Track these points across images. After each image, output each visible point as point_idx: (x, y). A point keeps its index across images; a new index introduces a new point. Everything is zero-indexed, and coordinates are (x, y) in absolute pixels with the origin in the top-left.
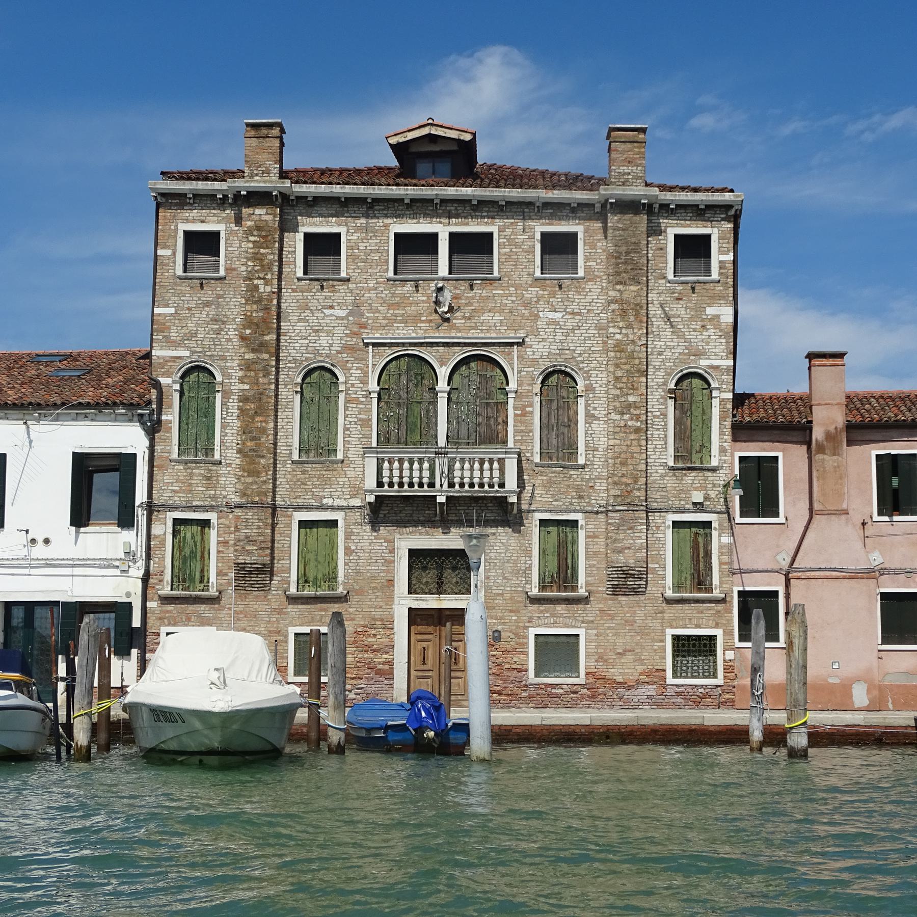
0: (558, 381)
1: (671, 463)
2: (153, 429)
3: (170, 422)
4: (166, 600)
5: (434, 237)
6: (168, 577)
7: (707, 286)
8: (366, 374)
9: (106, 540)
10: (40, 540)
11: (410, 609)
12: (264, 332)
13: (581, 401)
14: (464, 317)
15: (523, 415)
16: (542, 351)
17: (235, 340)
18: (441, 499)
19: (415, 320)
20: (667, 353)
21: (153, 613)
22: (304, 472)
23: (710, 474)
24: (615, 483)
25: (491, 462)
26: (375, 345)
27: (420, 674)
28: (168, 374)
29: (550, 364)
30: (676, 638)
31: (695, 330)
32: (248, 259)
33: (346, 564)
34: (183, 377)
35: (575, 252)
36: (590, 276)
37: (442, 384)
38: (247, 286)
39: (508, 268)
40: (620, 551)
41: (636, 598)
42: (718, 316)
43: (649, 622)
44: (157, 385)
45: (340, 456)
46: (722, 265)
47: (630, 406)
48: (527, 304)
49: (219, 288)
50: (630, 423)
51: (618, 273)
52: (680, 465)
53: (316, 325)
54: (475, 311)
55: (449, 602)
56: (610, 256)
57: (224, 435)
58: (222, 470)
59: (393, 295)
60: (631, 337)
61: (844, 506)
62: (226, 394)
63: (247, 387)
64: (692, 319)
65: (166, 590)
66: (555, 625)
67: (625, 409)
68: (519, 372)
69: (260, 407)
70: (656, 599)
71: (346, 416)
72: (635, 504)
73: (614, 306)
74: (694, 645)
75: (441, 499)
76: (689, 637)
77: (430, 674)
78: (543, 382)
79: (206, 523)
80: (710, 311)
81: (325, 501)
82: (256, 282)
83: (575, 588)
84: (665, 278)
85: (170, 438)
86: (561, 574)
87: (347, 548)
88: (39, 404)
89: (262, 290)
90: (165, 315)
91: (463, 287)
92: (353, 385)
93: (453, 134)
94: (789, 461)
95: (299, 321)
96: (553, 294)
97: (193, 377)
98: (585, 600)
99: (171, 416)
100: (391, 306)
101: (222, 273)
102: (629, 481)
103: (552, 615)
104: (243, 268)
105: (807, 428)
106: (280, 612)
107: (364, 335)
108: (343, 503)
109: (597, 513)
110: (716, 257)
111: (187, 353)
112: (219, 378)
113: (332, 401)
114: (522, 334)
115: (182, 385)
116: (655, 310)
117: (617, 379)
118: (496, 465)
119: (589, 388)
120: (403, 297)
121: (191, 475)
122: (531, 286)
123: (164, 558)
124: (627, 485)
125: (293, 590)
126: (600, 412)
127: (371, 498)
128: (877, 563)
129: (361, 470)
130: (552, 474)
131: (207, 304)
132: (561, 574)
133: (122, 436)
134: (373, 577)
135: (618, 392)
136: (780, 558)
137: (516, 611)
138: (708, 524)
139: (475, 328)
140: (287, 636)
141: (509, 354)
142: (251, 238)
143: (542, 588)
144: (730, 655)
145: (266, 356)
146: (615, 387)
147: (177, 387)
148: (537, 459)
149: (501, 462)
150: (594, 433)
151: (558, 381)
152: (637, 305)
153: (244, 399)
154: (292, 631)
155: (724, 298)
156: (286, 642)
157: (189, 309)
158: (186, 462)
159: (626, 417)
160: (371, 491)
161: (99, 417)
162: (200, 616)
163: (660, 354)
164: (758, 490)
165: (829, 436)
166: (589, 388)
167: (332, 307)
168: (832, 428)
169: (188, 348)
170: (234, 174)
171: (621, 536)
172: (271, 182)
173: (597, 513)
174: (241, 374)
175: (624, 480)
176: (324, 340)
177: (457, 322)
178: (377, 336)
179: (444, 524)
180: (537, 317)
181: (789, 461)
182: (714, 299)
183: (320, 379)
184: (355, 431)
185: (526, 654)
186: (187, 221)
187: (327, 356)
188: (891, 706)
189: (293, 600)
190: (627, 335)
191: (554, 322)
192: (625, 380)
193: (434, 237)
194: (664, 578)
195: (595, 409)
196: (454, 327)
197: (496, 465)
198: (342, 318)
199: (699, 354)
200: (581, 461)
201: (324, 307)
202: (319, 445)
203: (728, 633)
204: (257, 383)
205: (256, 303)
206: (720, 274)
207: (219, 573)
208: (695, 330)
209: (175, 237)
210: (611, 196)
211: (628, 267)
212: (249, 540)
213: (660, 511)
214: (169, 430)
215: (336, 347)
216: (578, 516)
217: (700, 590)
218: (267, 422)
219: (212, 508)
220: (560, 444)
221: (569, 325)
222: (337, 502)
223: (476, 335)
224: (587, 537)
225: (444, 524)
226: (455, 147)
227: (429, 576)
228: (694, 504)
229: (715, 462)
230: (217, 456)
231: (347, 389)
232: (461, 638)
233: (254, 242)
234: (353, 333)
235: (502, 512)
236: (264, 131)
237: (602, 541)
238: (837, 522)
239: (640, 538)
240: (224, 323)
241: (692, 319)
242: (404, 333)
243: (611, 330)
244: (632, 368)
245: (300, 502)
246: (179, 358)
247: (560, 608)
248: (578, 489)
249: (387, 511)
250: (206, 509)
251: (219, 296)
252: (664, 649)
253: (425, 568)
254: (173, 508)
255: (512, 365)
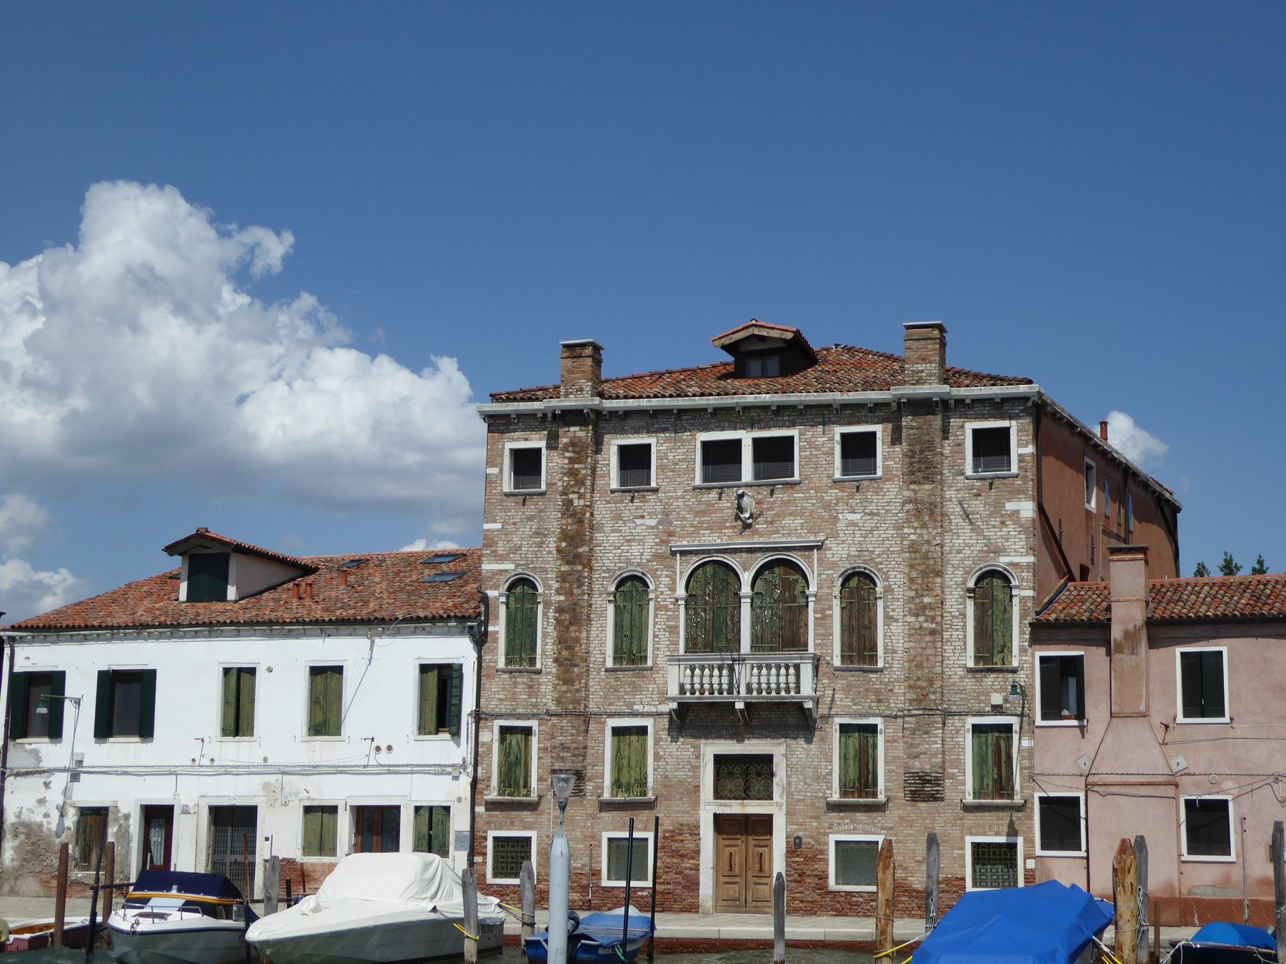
0: (858, 585)
1: (971, 664)
2: (481, 640)
3: (497, 632)
4: (491, 806)
5: (737, 443)
6: (495, 781)
7: (1006, 481)
8: (674, 581)
9: (443, 749)
10: (384, 747)
11: (716, 815)
12: (576, 544)
13: (880, 603)
14: (766, 522)
15: (824, 619)
16: (841, 553)
17: (554, 550)
18: (740, 705)
19: (720, 527)
20: (963, 551)
21: (481, 817)
22: (617, 679)
23: (1010, 675)
24: (910, 687)
25: (787, 667)
26: (683, 553)
27: (727, 880)
28: (496, 587)
29: (849, 566)
30: (976, 846)
31: (994, 527)
32: (564, 474)
33: (655, 770)
34: (509, 589)
35: (873, 454)
36: (888, 477)
37: (746, 590)
38: (563, 501)
39: (808, 471)
40: (916, 757)
41: (936, 804)
42: (1017, 512)
43: (949, 829)
44: (485, 599)
45: (650, 663)
46: (1021, 458)
47: (924, 607)
48: (827, 507)
49: (540, 502)
50: (925, 625)
51: (912, 473)
52: (981, 666)
53: (628, 535)
54: (776, 515)
55: (754, 807)
56: (905, 455)
57: (544, 644)
58: (543, 679)
59: (700, 502)
60: (926, 537)
61: (1143, 708)
62: (547, 605)
63: (562, 598)
64: (991, 515)
65: (493, 795)
66: (855, 831)
67: (919, 611)
68: (819, 575)
69: (573, 617)
70: (956, 805)
71: (655, 623)
72: (929, 707)
73: (908, 506)
74: (994, 853)
75: (740, 705)
76: (989, 845)
77: (737, 879)
78: (843, 585)
79: (527, 731)
80: (1010, 506)
81: (636, 707)
82: (571, 496)
83: (875, 795)
84: (963, 474)
85: (496, 648)
86: (861, 780)
87: (656, 755)
88: (383, 619)
89: (576, 504)
90: (493, 531)
91: (765, 492)
92: (662, 593)
93: (775, 334)
94: (1094, 659)
95: (613, 531)
96: (851, 496)
97: (519, 589)
98: (880, 808)
99: (499, 628)
100: (697, 513)
101: (543, 487)
102: (925, 685)
103: (853, 822)
104: (560, 484)
105: (1106, 626)
106: (594, 817)
107: (672, 544)
108: (653, 709)
109: (896, 717)
110: (1015, 451)
111: (512, 566)
112: (540, 590)
113: (643, 608)
114: (821, 537)
115: (508, 597)
116: (953, 508)
117: (912, 580)
118: (792, 671)
119: (888, 590)
120: (709, 504)
121: (515, 684)
122: (830, 488)
123: (491, 764)
124: (922, 688)
125: (607, 795)
126: (898, 613)
127: (674, 705)
128: (1180, 768)
129: (672, 676)
130: (852, 678)
131: (530, 518)
132: (861, 780)
133: (455, 649)
134: (681, 782)
135: (913, 594)
136: (1081, 762)
137: (816, 818)
138: (1008, 728)
139: (777, 532)
140: (600, 841)
141: (810, 557)
142: (567, 455)
143: (844, 793)
144: (1031, 864)
145: (579, 568)
146: (910, 589)
147: (503, 599)
148: (837, 662)
149: (797, 667)
150: (892, 634)
151: (858, 585)
152: (931, 504)
153: (560, 610)
154: (605, 836)
155: (1023, 492)
156: (600, 846)
157: (514, 524)
158: (510, 672)
159: (921, 619)
160: (673, 699)
161: (435, 630)
162: (522, 821)
163: (959, 552)
164: (1063, 689)
165: (1127, 635)
166: (888, 590)
167: (642, 517)
168: (1131, 627)
169: (513, 561)
170: (555, 392)
171: (918, 741)
172: (583, 399)
173: (896, 717)
174: (557, 585)
175: (919, 683)
176: (636, 549)
177: (760, 526)
178: (684, 544)
179: (742, 731)
180: (836, 519)
181: (1094, 659)
182: (1014, 494)
183: (632, 588)
184: (664, 637)
185: (826, 861)
186: (513, 440)
187: (639, 565)
188: (1196, 921)
189: (605, 806)
190: (921, 535)
191: (853, 524)
192: (919, 581)
193: (737, 443)
194: (963, 783)
195: (893, 610)
196: (757, 532)
197: (792, 671)
198: (652, 528)
199: (998, 551)
200: (880, 664)
201: (636, 517)
202: (631, 651)
203: (1029, 841)
204: (571, 594)
205: (571, 516)
206: (1020, 468)
207: (540, 779)
208: (994, 527)
209: (502, 455)
210: (902, 396)
211: (922, 467)
212: (564, 747)
213: (959, 714)
214: (496, 640)
215: (647, 556)
216: (878, 721)
217: (1002, 796)
218: (580, 632)
219: (534, 716)
220: (860, 646)
221: (868, 526)
222: (647, 709)
223: (778, 539)
224: (886, 741)
225: (742, 731)
226: (783, 345)
227: (736, 784)
228: (994, 707)
229: (1015, 664)
230: (538, 666)
231: (657, 597)
232: (769, 846)
233: (569, 458)
234: (663, 541)
235: (793, 719)
236: (578, 350)
237: (900, 745)
238: (1135, 726)
239: (936, 743)
240: (545, 536)
241: (991, 515)
242: (710, 539)
243: (906, 531)
244: (926, 569)
245: (612, 709)
246: (506, 571)
247: (860, 816)
248: (878, 692)
249: (692, 718)
250: (528, 717)
251: (541, 511)
252: (963, 857)
253: (730, 774)
254: (500, 716)
255: (812, 568)
